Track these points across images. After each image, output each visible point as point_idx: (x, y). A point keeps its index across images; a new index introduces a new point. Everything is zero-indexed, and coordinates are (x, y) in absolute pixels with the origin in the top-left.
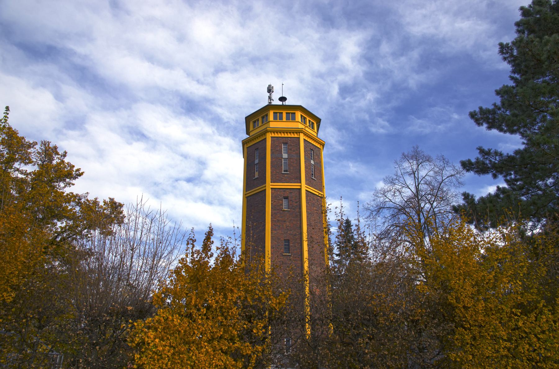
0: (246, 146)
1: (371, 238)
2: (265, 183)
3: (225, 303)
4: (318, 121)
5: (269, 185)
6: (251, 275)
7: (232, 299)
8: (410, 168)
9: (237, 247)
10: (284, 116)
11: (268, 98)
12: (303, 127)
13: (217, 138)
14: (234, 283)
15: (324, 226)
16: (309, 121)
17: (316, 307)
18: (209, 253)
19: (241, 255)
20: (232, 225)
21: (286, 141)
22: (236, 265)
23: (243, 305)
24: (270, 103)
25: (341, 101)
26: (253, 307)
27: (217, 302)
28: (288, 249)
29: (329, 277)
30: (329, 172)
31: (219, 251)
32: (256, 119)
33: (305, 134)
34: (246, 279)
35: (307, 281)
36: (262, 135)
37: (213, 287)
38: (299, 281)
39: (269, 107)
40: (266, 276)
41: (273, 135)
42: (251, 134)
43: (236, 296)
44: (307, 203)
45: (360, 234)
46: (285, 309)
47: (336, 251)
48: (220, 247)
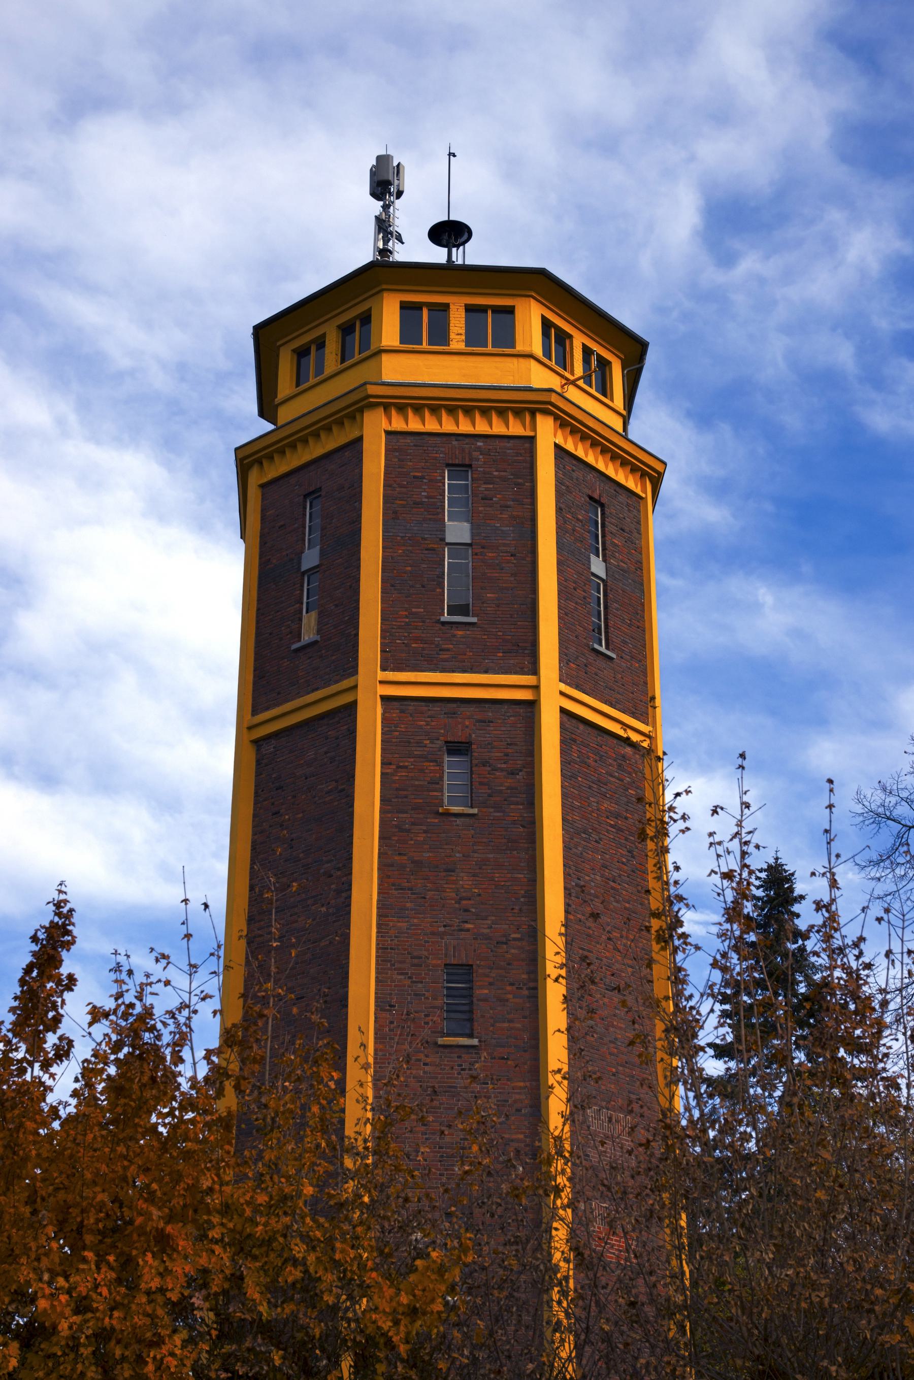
0: (255, 478)
1: (896, 972)
2: (353, 670)
3: (126, 1307)
4: (633, 349)
5: (375, 684)
6: (269, 1156)
7: (162, 1290)
8: (218, 1249)
9: (197, 1014)
10: (457, 322)
11: (372, 226)
12: (554, 382)
13: (80, 450)
14: (177, 1202)
15: (655, 904)
16: (587, 352)
17: (607, 1338)
18: (51, 1039)
19: (218, 1052)
20: (167, 895)
21: (460, 456)
22: (188, 1104)
23: (223, 1319)
24: (385, 252)
25: (713, 276)
26: (270, 1331)
27: (82, 1306)
28: (463, 1014)
29: (670, 1171)
30: (678, 623)
31: (101, 1029)
32: (301, 341)
33: (567, 422)
34: (240, 1179)
35: (558, 1190)
36: (340, 423)
37: (61, 1225)
38: (516, 1193)
39: (381, 273)
40: (348, 1163)
41: (398, 424)
42: (285, 414)
43: (181, 1268)
44: (568, 775)
45: (841, 950)
46: (444, 1344)
47: (712, 1030)
48: (110, 1004)
